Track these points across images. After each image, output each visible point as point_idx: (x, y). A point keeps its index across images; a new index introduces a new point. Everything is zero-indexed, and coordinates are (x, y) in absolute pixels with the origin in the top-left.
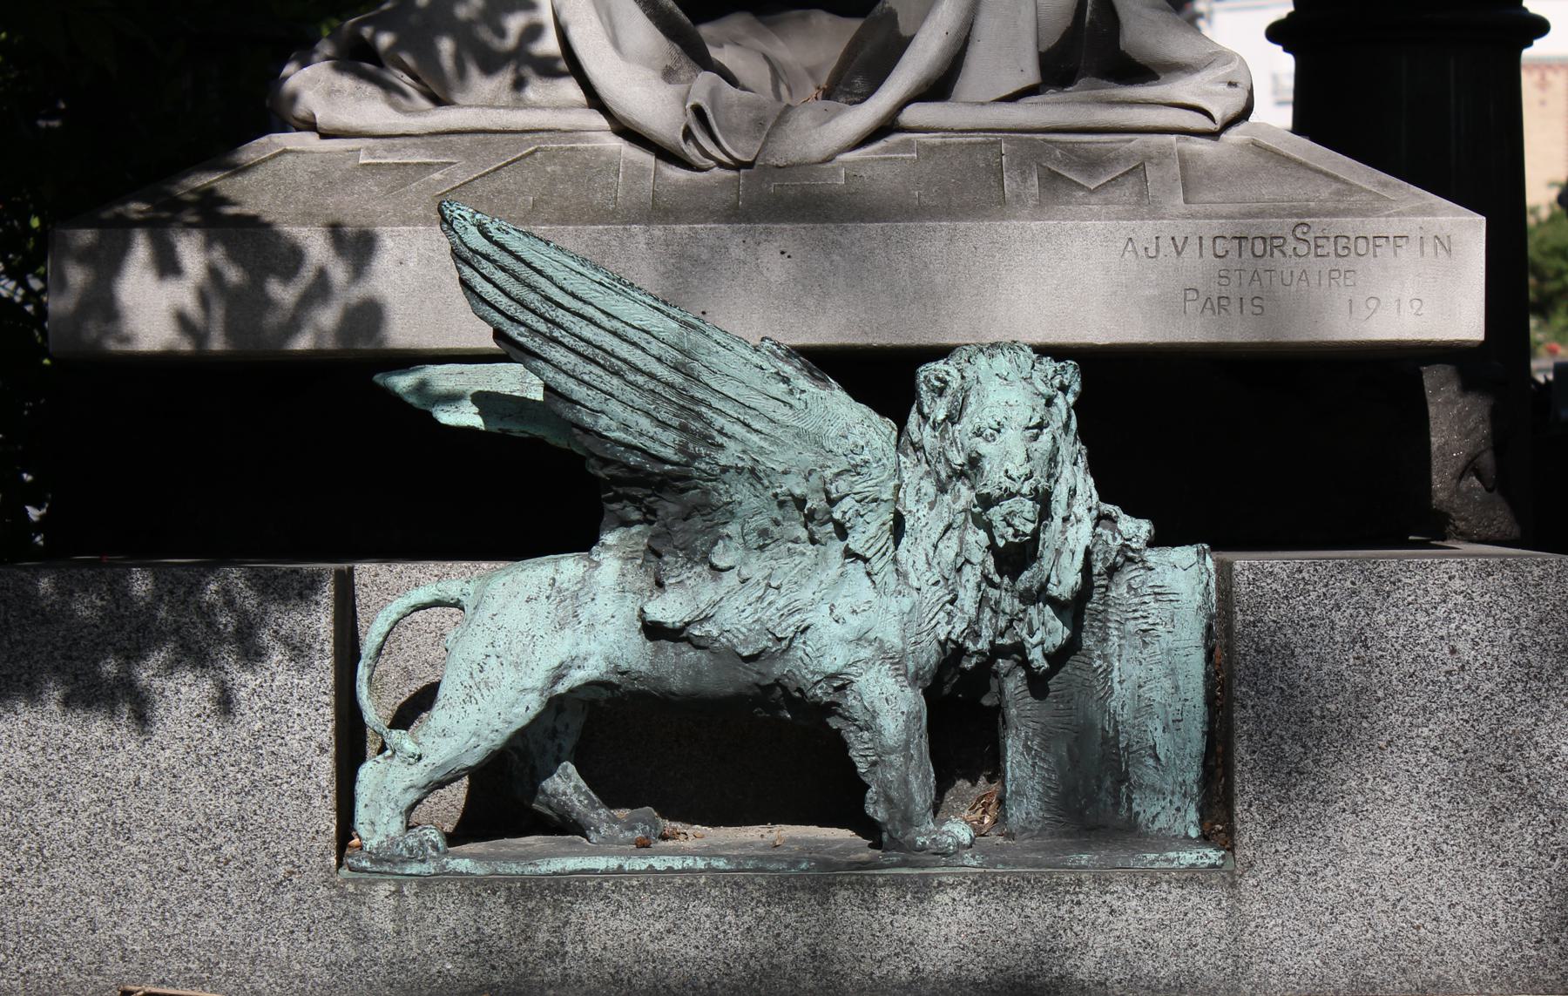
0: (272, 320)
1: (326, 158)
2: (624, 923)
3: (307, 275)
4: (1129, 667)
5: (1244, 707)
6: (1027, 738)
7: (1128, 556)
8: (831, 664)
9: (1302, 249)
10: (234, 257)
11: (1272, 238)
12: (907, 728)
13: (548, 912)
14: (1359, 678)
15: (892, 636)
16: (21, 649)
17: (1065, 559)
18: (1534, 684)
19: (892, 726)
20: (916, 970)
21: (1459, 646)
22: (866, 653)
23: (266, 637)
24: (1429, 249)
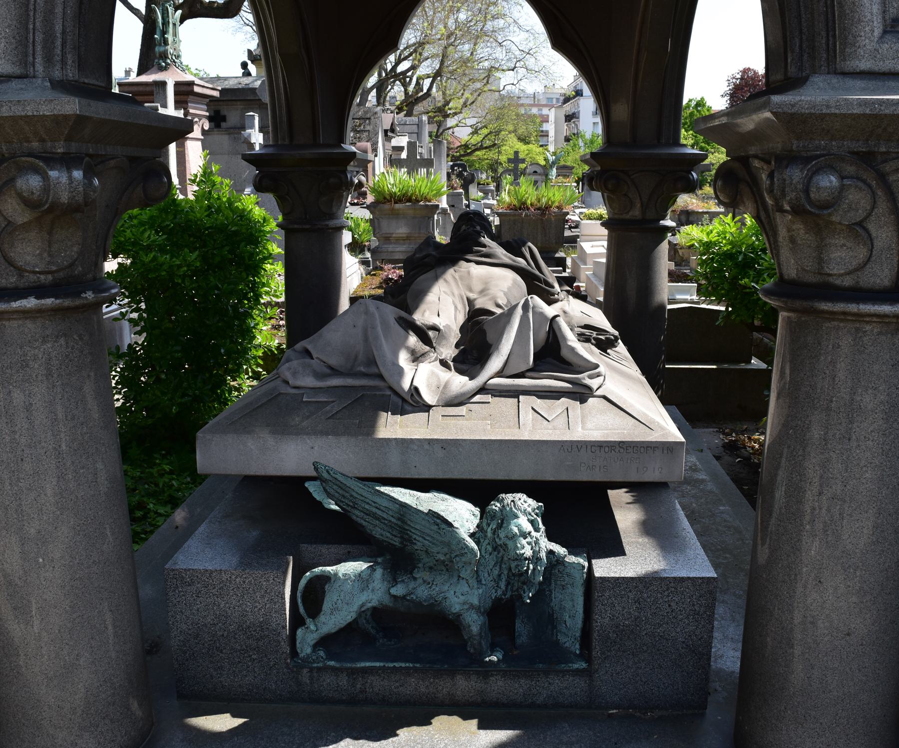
4: (558, 594)
5: (597, 622)
6: (523, 618)
9: (622, 450)
11: (611, 446)
12: (481, 628)
13: (360, 679)
14: (636, 614)
15: (476, 602)
16: (182, 593)
18: (696, 616)
19: (475, 629)
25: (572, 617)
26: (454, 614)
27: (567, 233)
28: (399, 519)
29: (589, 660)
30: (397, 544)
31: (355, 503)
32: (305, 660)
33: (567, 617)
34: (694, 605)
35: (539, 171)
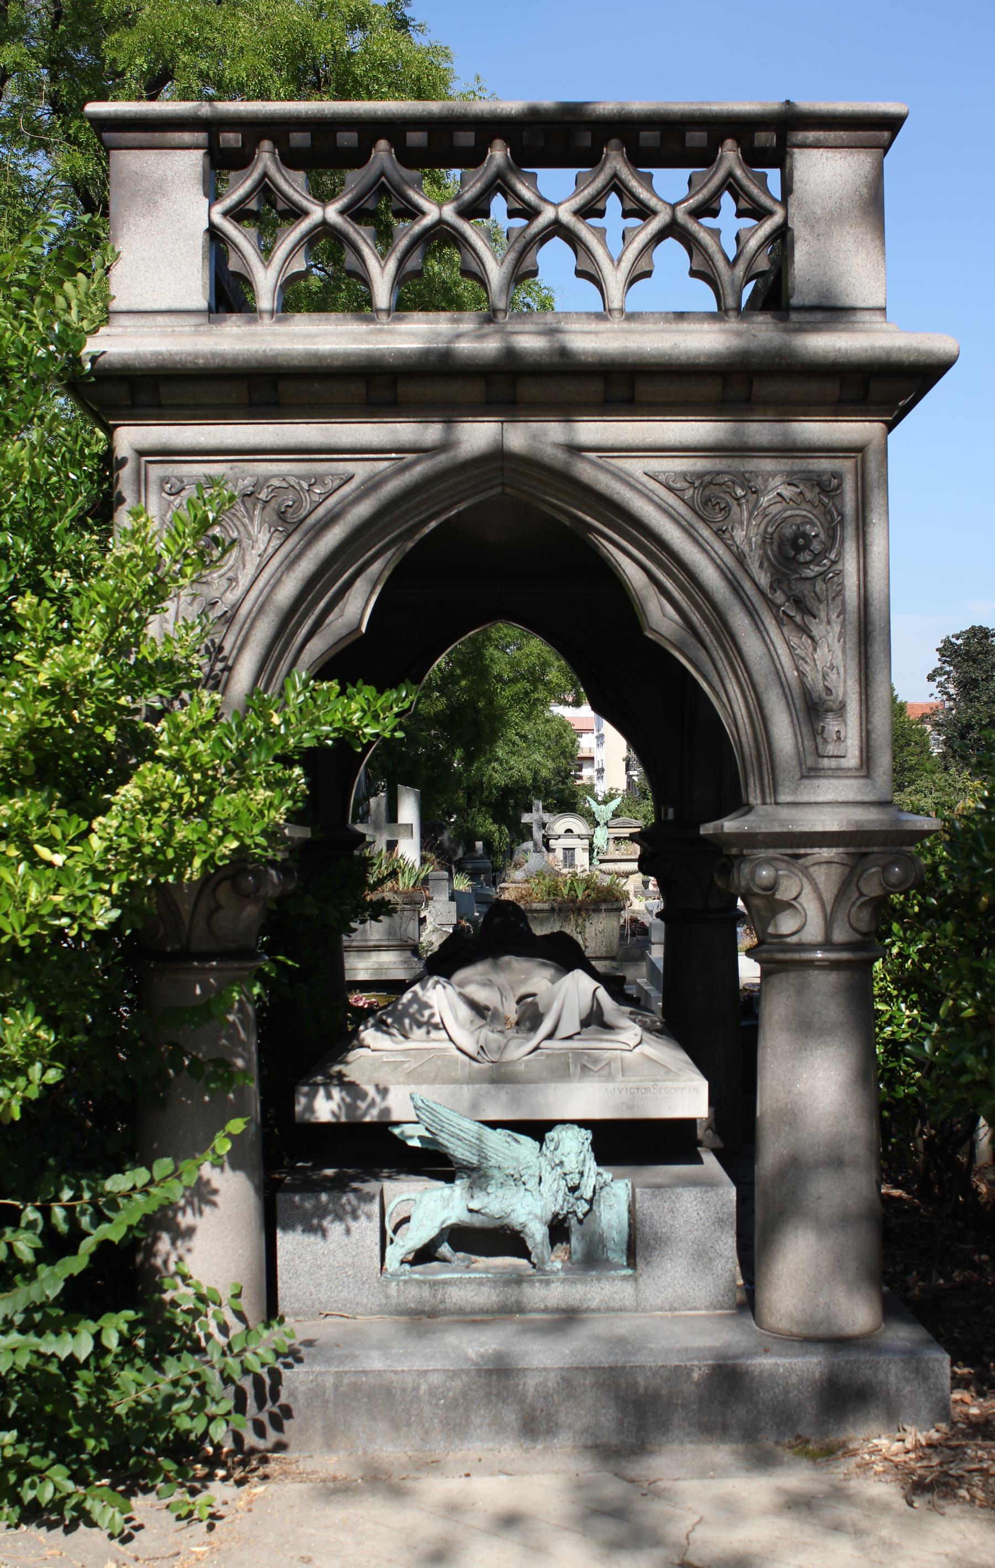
0: (359, 1112)
1: (374, 1058)
2: (462, 1293)
3: (369, 1100)
7: (606, 1184)
8: (521, 1220)
10: (348, 1094)
15: (539, 1213)
23: (360, 1212)
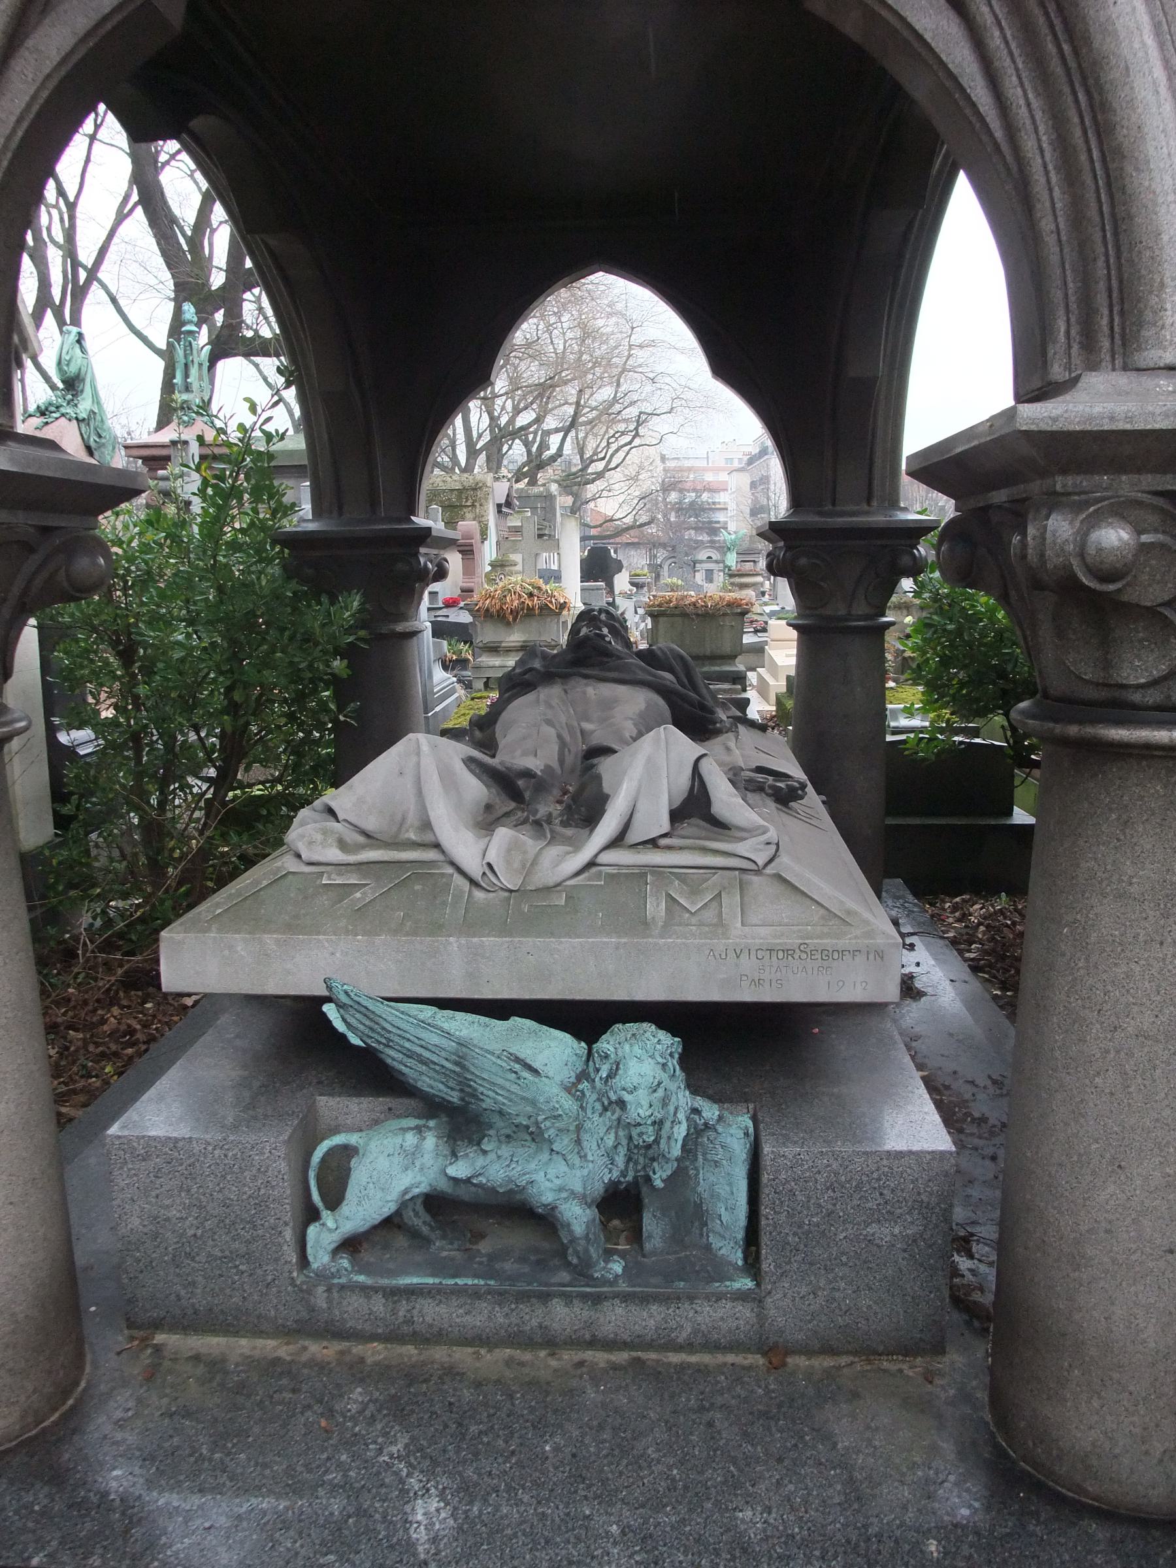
2: (443, 1309)
9: (804, 956)
12: (587, 1227)
14: (830, 1207)
15: (578, 1188)
17: (673, 1143)
19: (579, 1229)
20: (594, 1335)
21: (885, 1192)
22: (564, 1195)
24: (871, 957)
25: (731, 1209)
26: (545, 1206)
27: (748, 639)
28: (457, 1064)
29: (756, 1275)
30: (455, 1100)
31: (389, 1040)
32: (323, 1276)
33: (723, 1209)
34: (919, 1194)
35: (714, 558)
